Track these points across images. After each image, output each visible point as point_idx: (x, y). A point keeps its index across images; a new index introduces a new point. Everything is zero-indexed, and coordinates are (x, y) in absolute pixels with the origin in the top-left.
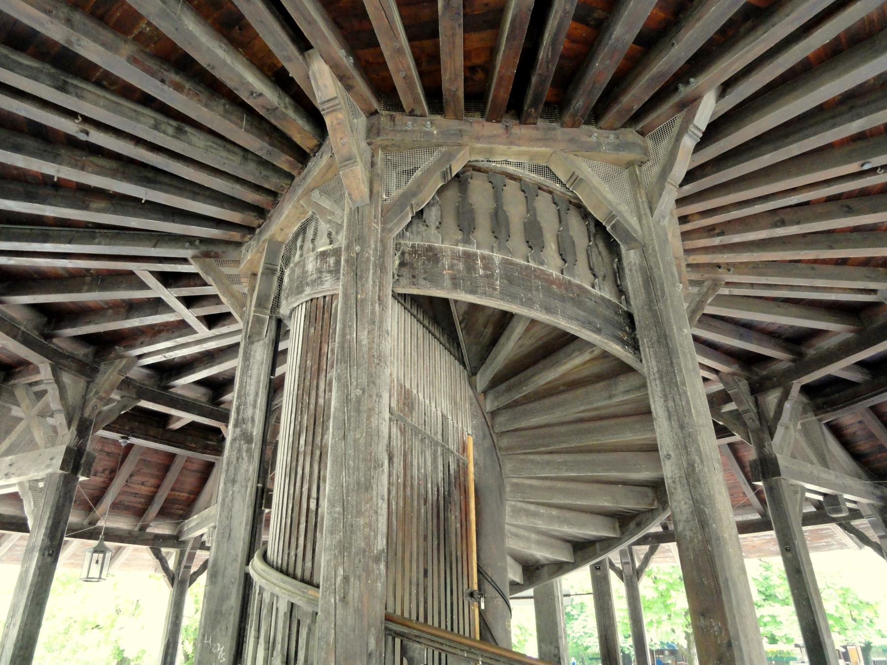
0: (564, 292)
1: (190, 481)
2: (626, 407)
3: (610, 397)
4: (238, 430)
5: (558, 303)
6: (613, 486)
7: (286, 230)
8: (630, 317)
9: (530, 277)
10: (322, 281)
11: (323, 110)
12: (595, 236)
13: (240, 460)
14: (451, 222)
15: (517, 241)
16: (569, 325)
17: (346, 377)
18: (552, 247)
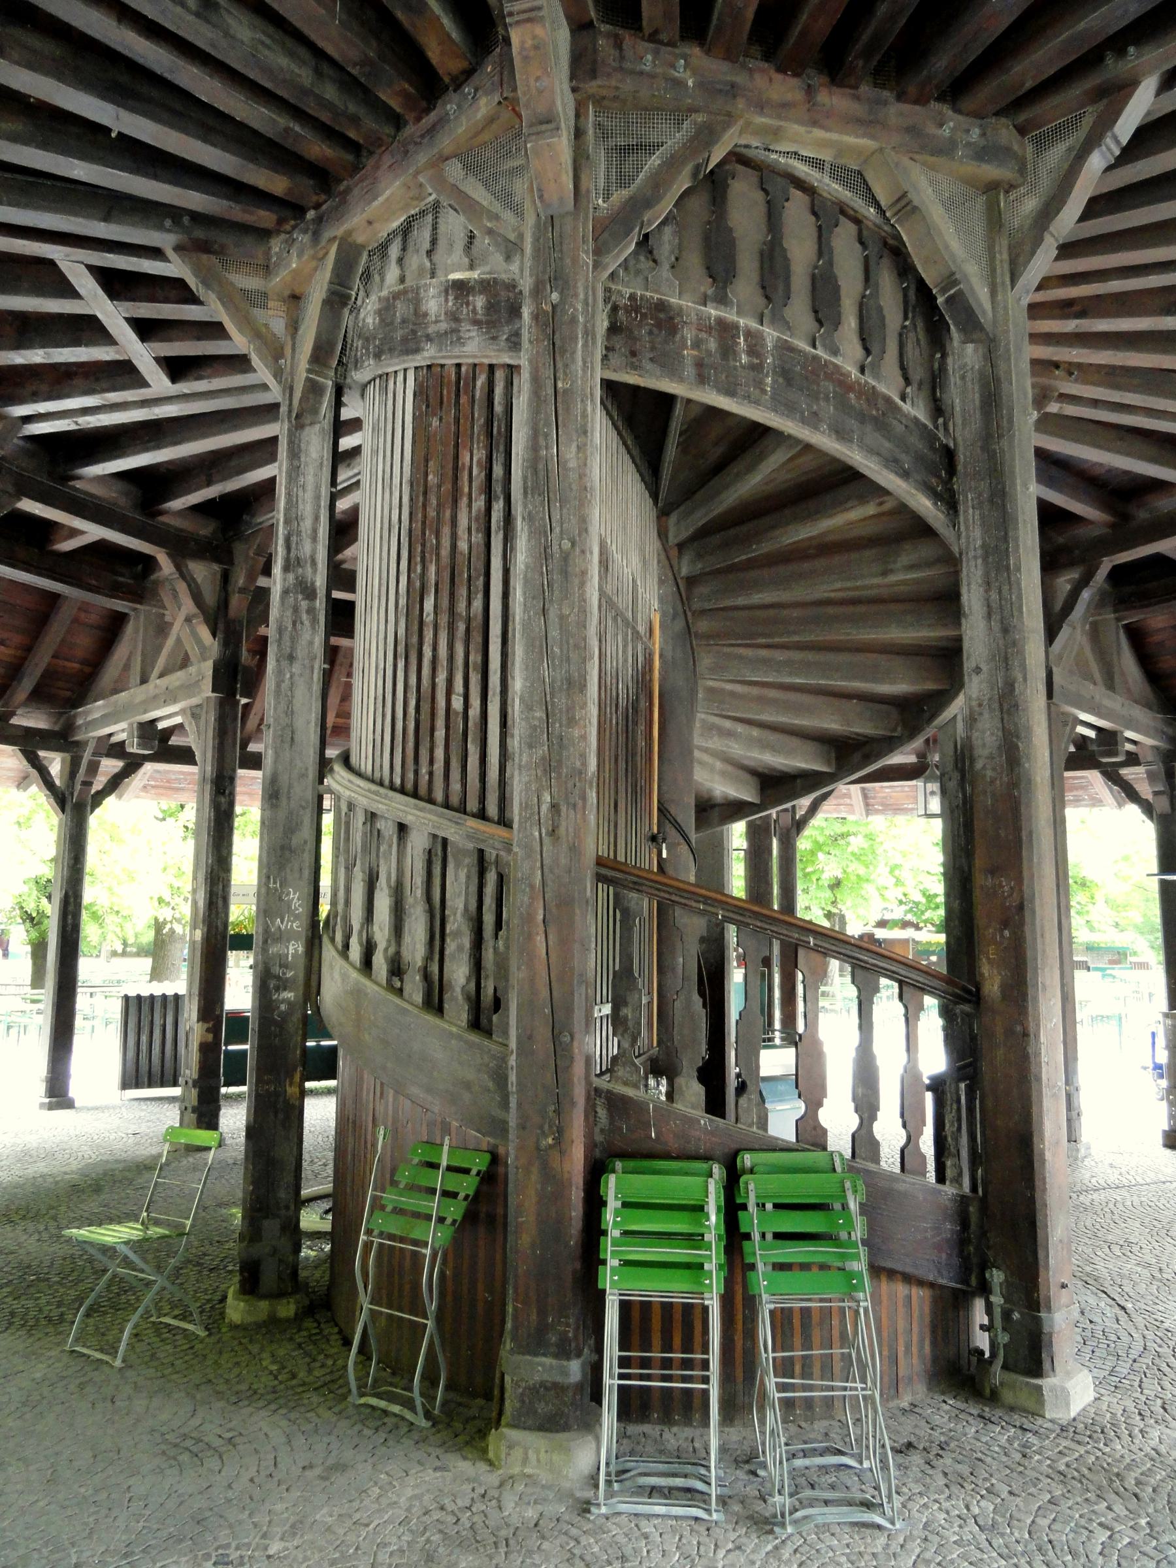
0: (865, 406)
1: (84, 642)
2: (902, 588)
3: (885, 573)
4: (291, 577)
5: (853, 424)
6: (844, 701)
7: (376, 225)
8: (949, 455)
9: (818, 376)
10: (459, 338)
11: (511, 14)
12: (914, 312)
13: (299, 626)
14: (694, 260)
15: (799, 309)
16: (866, 462)
17: (543, 519)
18: (850, 322)
